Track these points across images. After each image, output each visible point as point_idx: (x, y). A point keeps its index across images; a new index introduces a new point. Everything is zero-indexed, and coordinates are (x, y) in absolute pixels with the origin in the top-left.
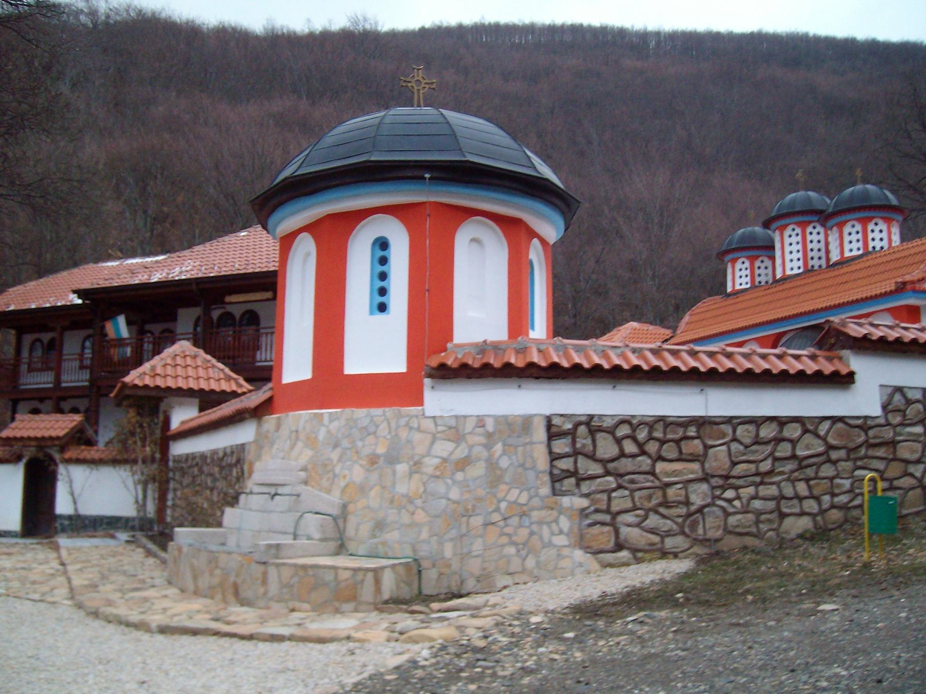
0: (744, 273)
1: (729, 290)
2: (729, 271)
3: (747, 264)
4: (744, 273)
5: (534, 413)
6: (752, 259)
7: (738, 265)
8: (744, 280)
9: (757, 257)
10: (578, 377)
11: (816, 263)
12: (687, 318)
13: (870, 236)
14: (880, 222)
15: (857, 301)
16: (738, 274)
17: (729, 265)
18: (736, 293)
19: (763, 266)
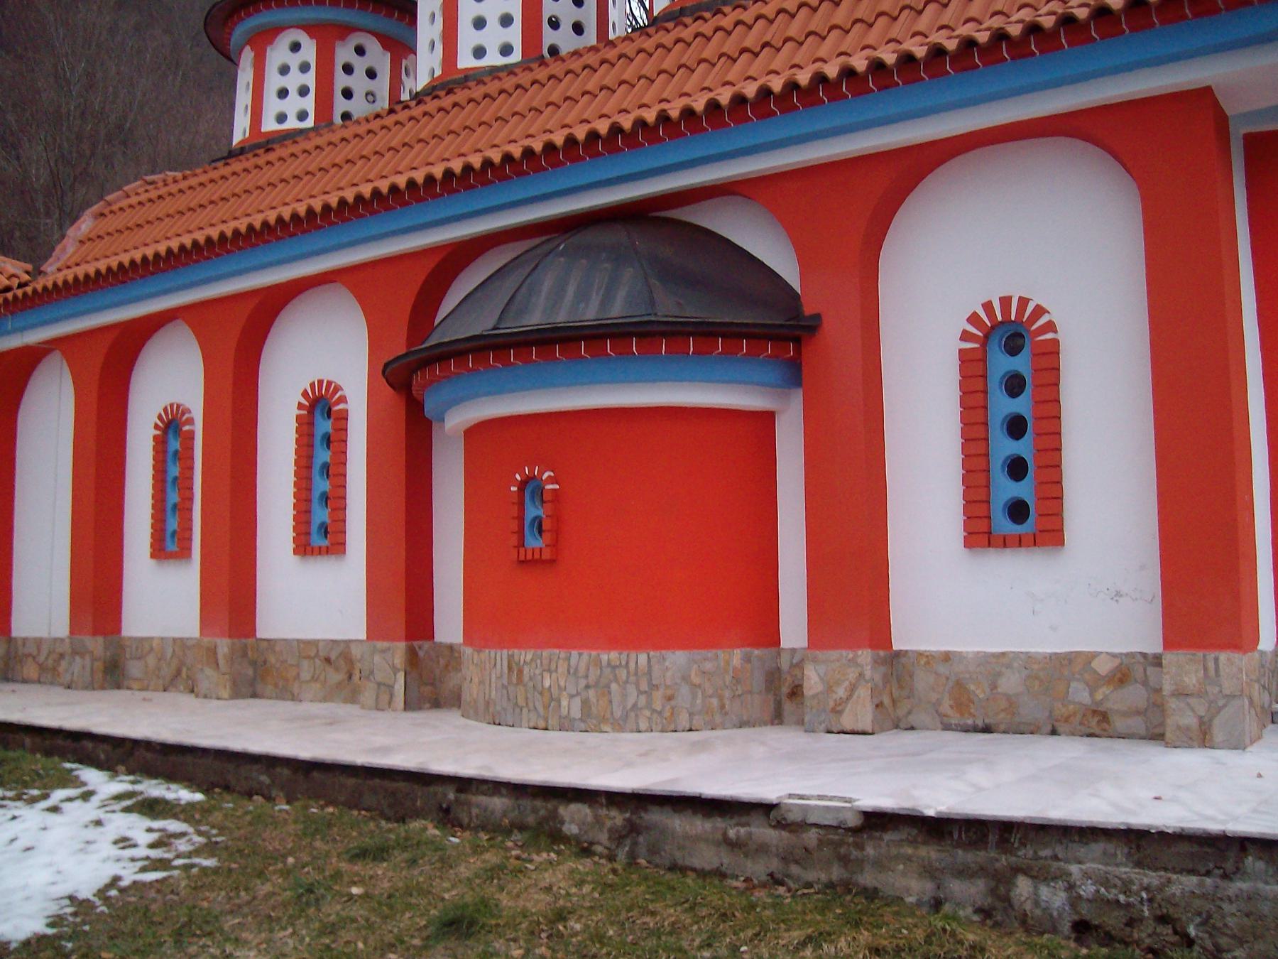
0: (294, 81)
1: (241, 129)
2: (245, 76)
3: (309, 51)
4: (294, 81)
5: (353, 638)
6: (327, 36)
7: (278, 53)
8: (293, 104)
9: (344, 31)
10: (654, 381)
11: (565, 40)
12: (85, 225)
13: (341, 80)
14: (373, 46)
15: (766, 104)
16: (274, 81)
17: (247, 56)
18: (263, 144)
19: (360, 65)
